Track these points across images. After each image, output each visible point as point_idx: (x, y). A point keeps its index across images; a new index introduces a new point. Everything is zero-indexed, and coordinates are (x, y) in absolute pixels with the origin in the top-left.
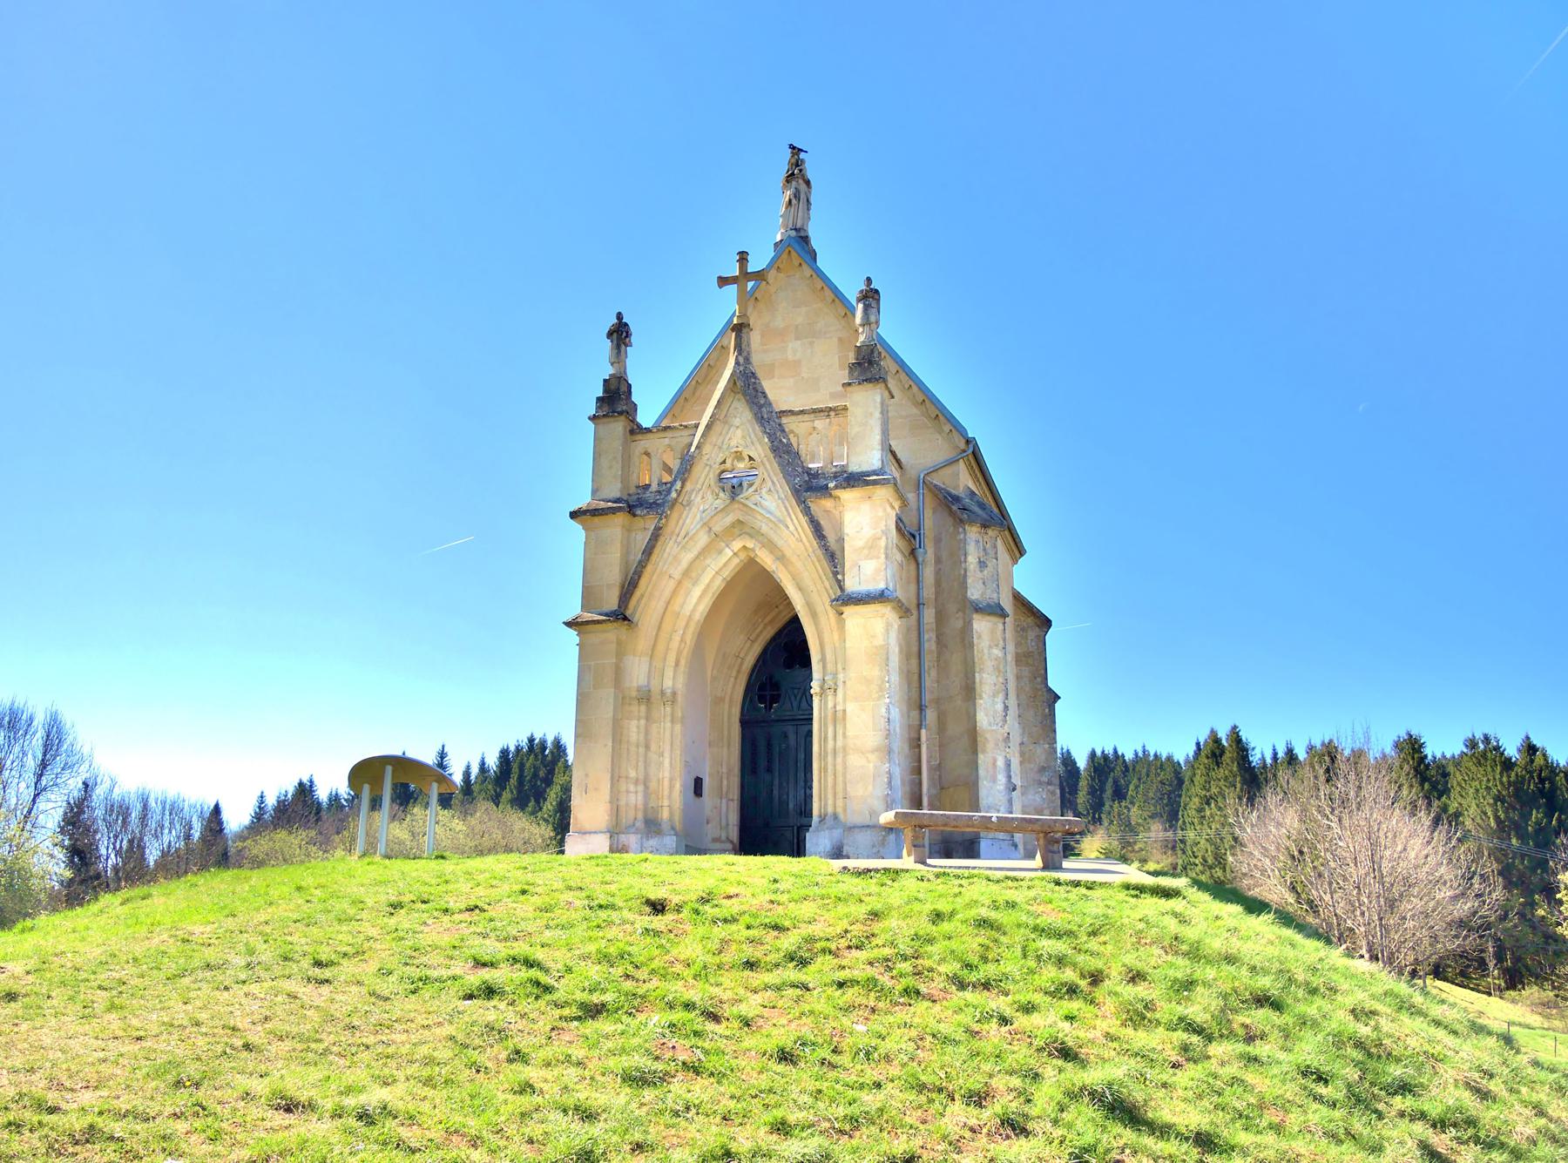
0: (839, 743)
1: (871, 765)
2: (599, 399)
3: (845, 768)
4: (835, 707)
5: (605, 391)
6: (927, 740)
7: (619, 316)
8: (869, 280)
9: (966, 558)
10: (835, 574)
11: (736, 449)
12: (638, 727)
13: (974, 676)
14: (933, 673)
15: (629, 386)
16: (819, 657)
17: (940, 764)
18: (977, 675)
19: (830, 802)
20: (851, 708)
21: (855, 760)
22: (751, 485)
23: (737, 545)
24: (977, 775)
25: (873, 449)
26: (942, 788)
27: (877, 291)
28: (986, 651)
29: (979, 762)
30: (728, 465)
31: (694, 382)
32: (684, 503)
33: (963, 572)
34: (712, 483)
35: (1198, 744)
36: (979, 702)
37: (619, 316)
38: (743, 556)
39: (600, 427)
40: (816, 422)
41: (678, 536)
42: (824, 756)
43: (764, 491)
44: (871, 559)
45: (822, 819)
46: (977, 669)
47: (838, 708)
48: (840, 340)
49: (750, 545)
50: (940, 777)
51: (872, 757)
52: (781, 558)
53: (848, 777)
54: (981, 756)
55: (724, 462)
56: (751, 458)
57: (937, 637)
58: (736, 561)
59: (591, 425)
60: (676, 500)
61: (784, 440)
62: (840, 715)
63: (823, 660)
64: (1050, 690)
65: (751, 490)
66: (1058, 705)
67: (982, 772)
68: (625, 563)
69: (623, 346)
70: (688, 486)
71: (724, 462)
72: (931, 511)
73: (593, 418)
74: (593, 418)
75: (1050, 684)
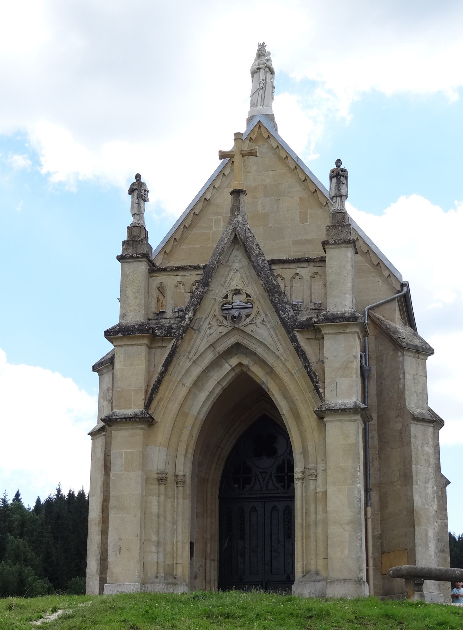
0: (319, 517)
1: (347, 534)
2: (124, 242)
3: (326, 537)
4: (315, 489)
5: (129, 236)
6: (372, 515)
7: (138, 177)
8: (339, 162)
9: (404, 376)
10: (317, 388)
11: (236, 288)
12: (159, 502)
13: (412, 467)
14: (376, 463)
15: (147, 233)
16: (301, 450)
17: (381, 535)
18: (414, 466)
19: (313, 562)
20: (331, 490)
21: (333, 530)
22: (247, 316)
23: (234, 361)
24: (414, 544)
25: (345, 293)
26: (383, 553)
27: (345, 171)
28: (420, 448)
29: (416, 533)
30: (229, 299)
31: (182, 227)
32: (195, 328)
33: (401, 387)
34: (217, 313)
35: (38, 501)
36: (415, 487)
37: (138, 177)
38: (238, 371)
39: (126, 265)
40: (299, 269)
41: (190, 353)
42: (306, 527)
43: (259, 321)
44: (346, 377)
45: (306, 573)
46: (414, 462)
47: (318, 490)
48: (301, 199)
49: (245, 361)
50: (382, 545)
51: (348, 528)
52: (271, 371)
53: (329, 542)
54: (417, 528)
55: (226, 296)
56: (248, 295)
57: (379, 436)
58: (233, 374)
59: (118, 264)
60: (189, 325)
61: (275, 283)
62: (320, 495)
63: (305, 452)
64: (443, 476)
65: (248, 320)
66: (448, 487)
67: (418, 541)
68: (149, 374)
69: (142, 201)
70: (198, 315)
71: (226, 296)
72: (373, 337)
73: (120, 258)
74: (120, 258)
75: (443, 472)
